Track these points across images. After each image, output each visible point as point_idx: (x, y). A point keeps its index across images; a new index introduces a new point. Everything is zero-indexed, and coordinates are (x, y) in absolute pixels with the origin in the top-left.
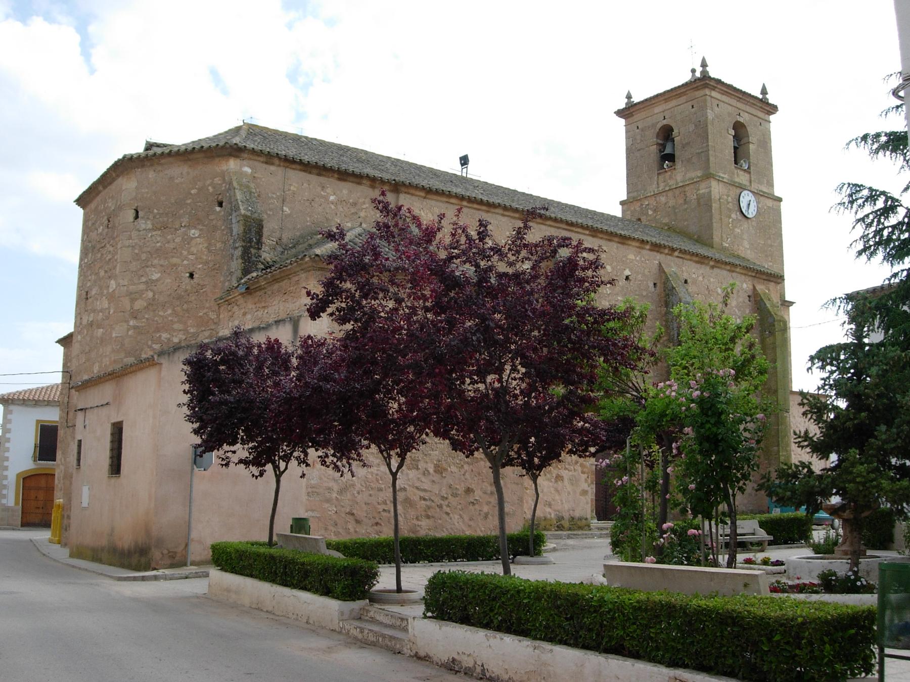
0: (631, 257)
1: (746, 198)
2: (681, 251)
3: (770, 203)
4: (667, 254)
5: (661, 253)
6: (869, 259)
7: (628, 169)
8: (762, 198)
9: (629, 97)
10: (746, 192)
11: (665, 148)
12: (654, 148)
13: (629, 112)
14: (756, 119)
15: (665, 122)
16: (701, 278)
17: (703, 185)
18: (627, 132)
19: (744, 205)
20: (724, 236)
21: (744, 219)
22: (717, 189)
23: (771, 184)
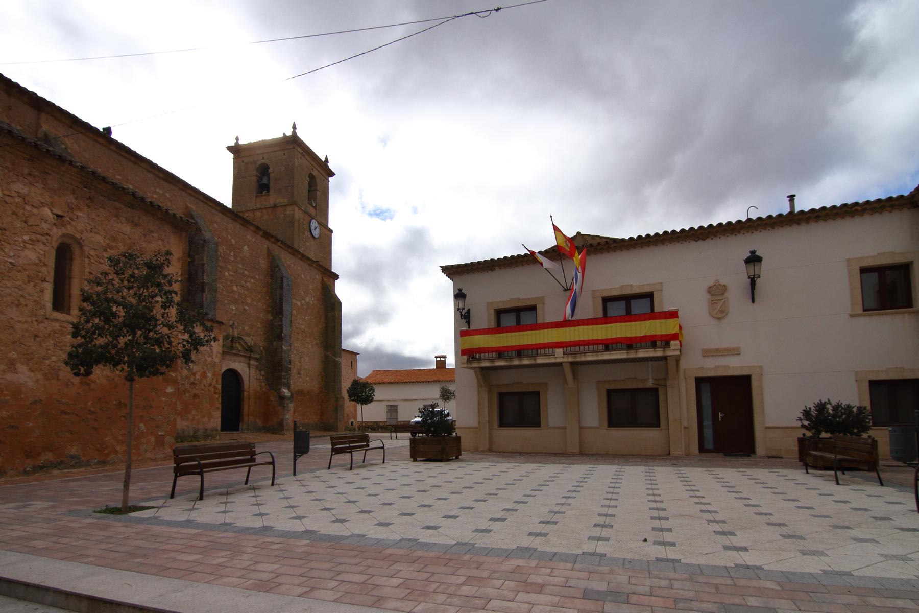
0: (249, 237)
1: (314, 224)
2: (282, 242)
3: (327, 232)
6: (81, 290)
9: (237, 139)
11: (262, 180)
12: (254, 179)
13: (236, 150)
15: (263, 161)
17: (289, 208)
19: (312, 228)
22: (298, 214)
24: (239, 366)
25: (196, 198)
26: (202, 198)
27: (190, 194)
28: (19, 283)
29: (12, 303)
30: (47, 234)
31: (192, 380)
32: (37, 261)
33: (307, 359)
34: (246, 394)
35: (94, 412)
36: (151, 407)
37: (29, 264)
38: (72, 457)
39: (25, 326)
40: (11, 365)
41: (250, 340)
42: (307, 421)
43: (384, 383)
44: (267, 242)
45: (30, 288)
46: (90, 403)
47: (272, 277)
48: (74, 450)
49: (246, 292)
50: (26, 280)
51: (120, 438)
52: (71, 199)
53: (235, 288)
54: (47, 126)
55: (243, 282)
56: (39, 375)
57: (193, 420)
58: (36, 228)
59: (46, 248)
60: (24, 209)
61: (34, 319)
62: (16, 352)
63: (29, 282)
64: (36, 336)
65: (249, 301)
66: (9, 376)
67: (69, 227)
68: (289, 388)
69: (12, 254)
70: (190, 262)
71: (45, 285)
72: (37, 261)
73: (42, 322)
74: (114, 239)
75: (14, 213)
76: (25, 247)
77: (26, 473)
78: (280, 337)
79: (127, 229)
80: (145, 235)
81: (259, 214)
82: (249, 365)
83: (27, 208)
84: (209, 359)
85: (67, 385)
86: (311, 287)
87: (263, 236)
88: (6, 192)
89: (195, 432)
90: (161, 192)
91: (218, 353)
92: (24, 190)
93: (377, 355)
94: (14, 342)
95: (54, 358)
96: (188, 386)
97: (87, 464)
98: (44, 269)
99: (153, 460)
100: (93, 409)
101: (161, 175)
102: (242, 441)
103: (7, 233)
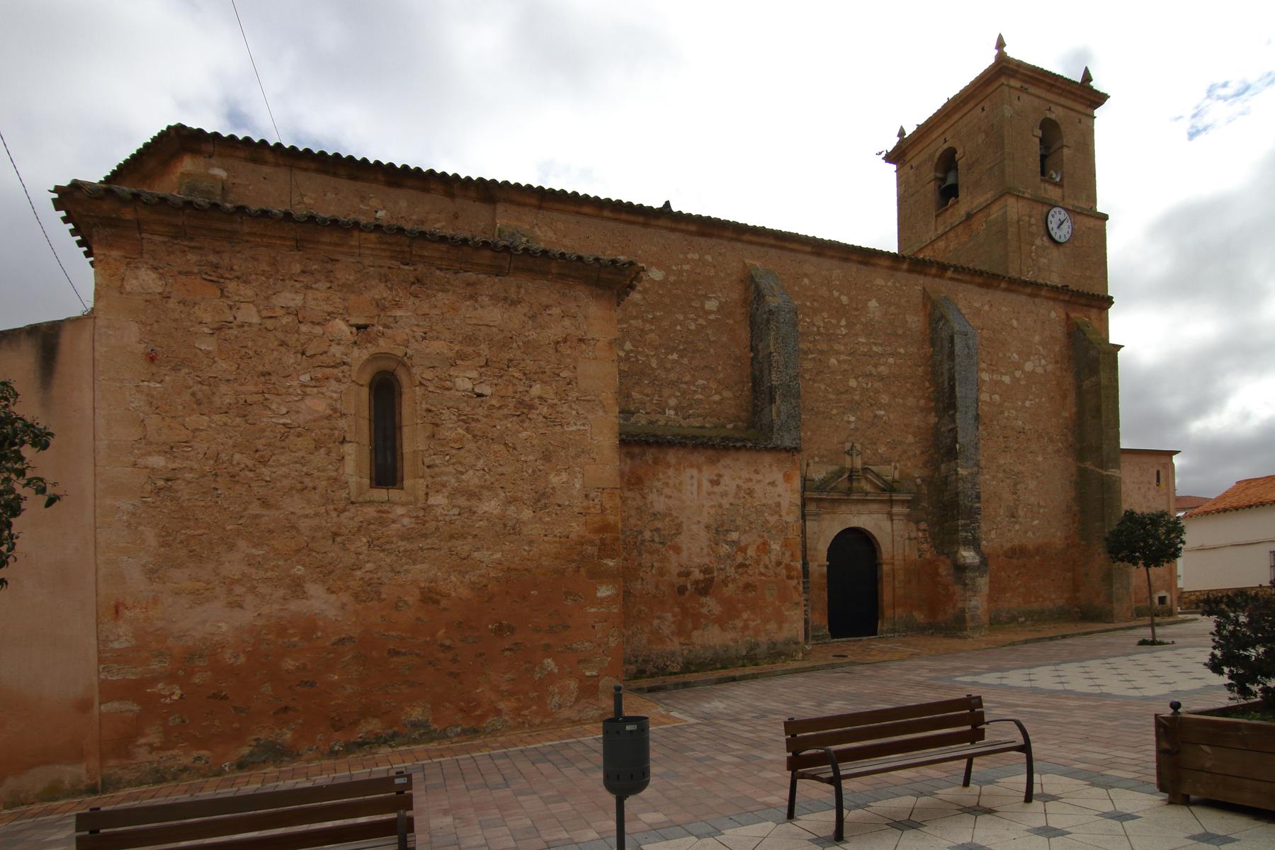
0: (880, 282)
3: (1091, 223)
4: (935, 276)
5: (926, 274)
7: (899, 205)
8: (1079, 218)
10: (1057, 209)
14: (1073, 114)
15: (945, 146)
16: (986, 308)
18: (898, 178)
19: (1053, 225)
20: (1025, 269)
21: (1052, 246)
23: (1092, 198)
24: (868, 519)
25: (763, 245)
26: (773, 242)
27: (751, 243)
28: (300, 454)
29: (291, 489)
30: (344, 363)
31: (740, 559)
32: (330, 412)
33: (1032, 484)
34: (885, 568)
35: (449, 648)
36: (567, 627)
37: (315, 421)
38: (415, 725)
39: (316, 522)
40: (297, 588)
41: (889, 472)
42: (1036, 606)
43: (1262, 504)
44: (922, 280)
45: (319, 458)
46: (441, 633)
47: (933, 343)
48: (416, 713)
49: (878, 385)
50: (312, 446)
51: (504, 687)
52: (379, 291)
53: (853, 383)
54: (505, 220)
55: (870, 368)
56: (345, 597)
57: (746, 627)
58: (324, 357)
59: (343, 387)
60: (297, 332)
61: (331, 507)
62: (303, 565)
63: (317, 448)
64: (335, 535)
65: (885, 399)
66: (294, 606)
67: (382, 342)
68: (977, 549)
69: (284, 410)
70: (752, 359)
71: (348, 448)
72: (330, 412)
73: (344, 510)
74: (470, 340)
75: (283, 344)
76: (305, 394)
77: (333, 754)
78: (951, 453)
79: (494, 315)
80: (533, 318)
81: (941, 244)
82: (891, 516)
83: (304, 328)
84: (773, 520)
85: (397, 607)
86: (1037, 338)
87: (909, 271)
88: (265, 313)
89: (751, 649)
90: (696, 256)
91: (791, 504)
92: (298, 300)
93: (1220, 450)
94: (299, 551)
95: (369, 566)
96: (731, 571)
97: (443, 736)
98: (342, 423)
99: (574, 722)
100: (448, 642)
101: (693, 228)
102: (381, 771)
103: (274, 379)
